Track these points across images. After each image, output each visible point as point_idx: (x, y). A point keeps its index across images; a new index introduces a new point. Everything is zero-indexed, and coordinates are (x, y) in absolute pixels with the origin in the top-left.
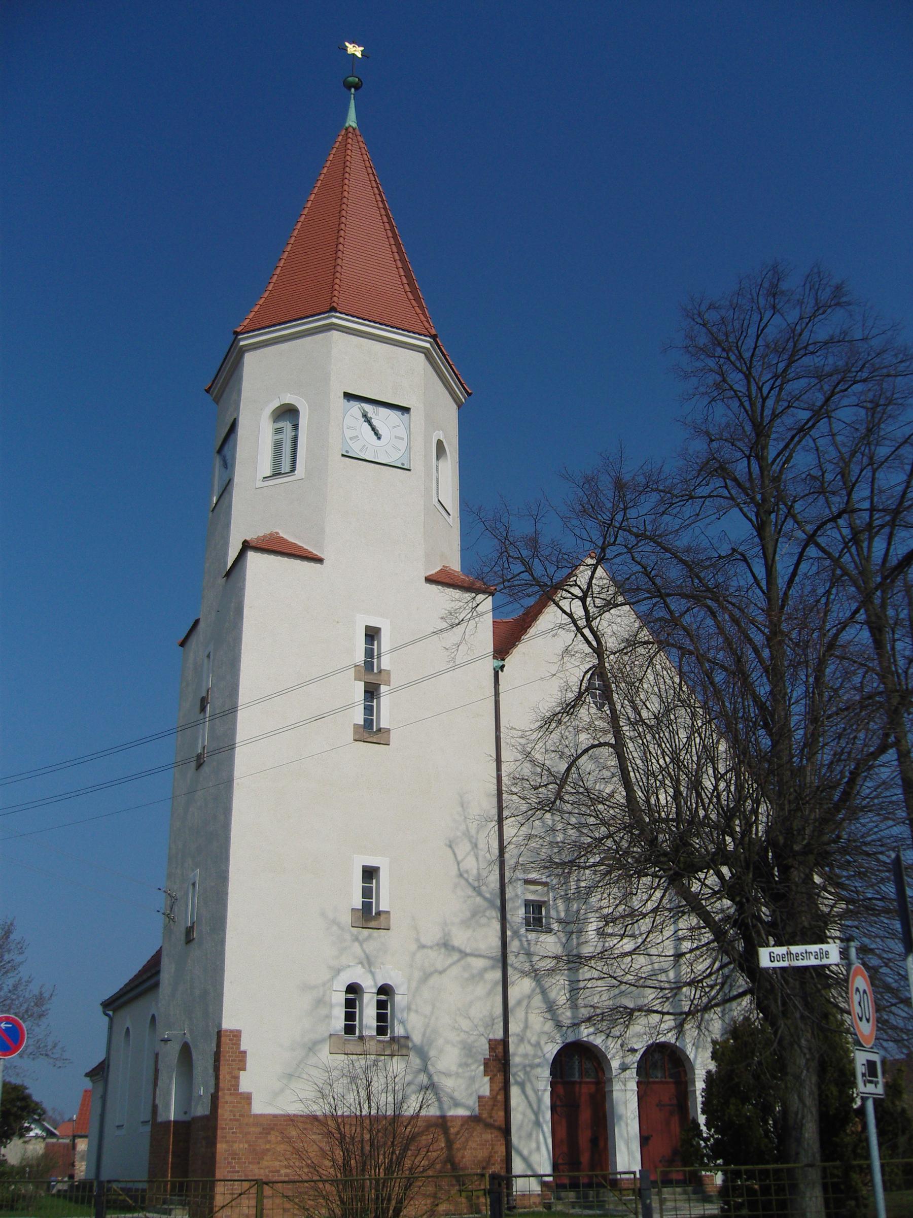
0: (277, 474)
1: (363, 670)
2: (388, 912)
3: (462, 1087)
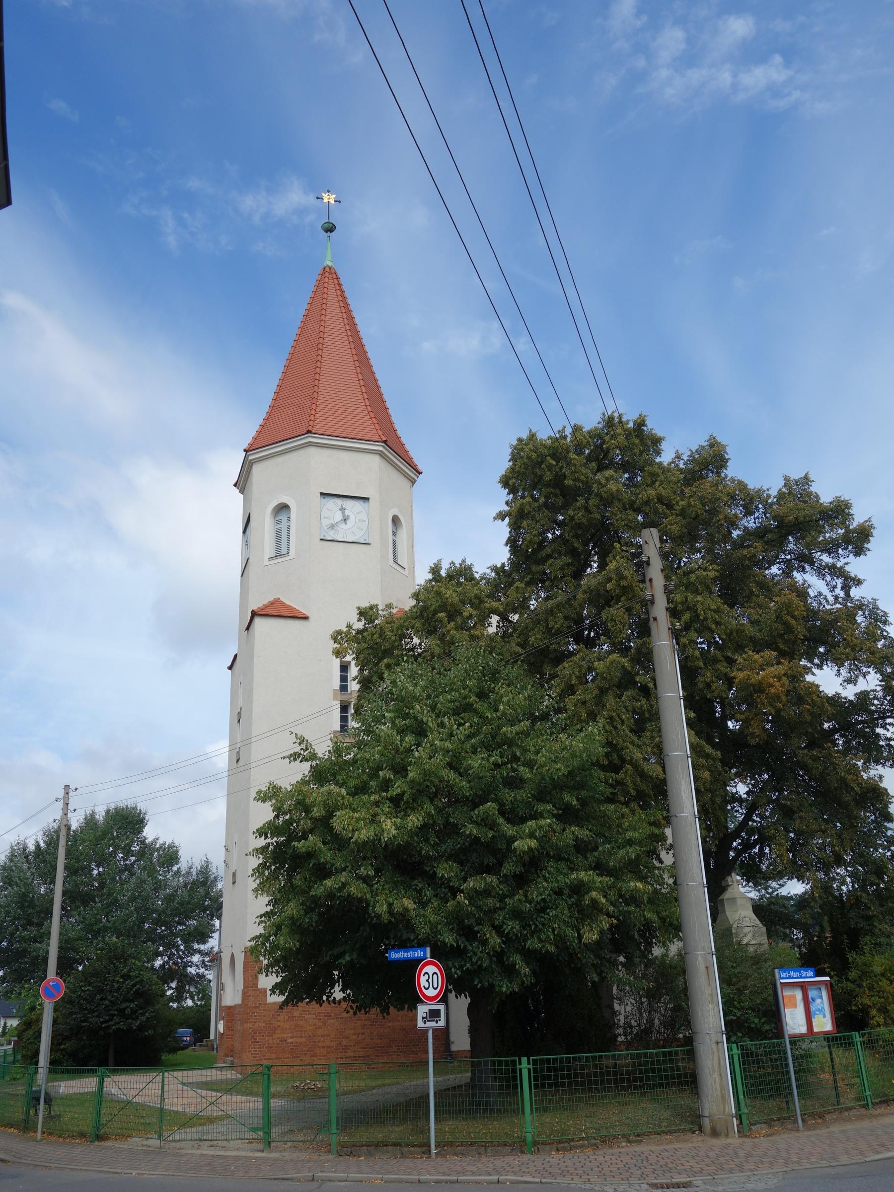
1: (338, 692)
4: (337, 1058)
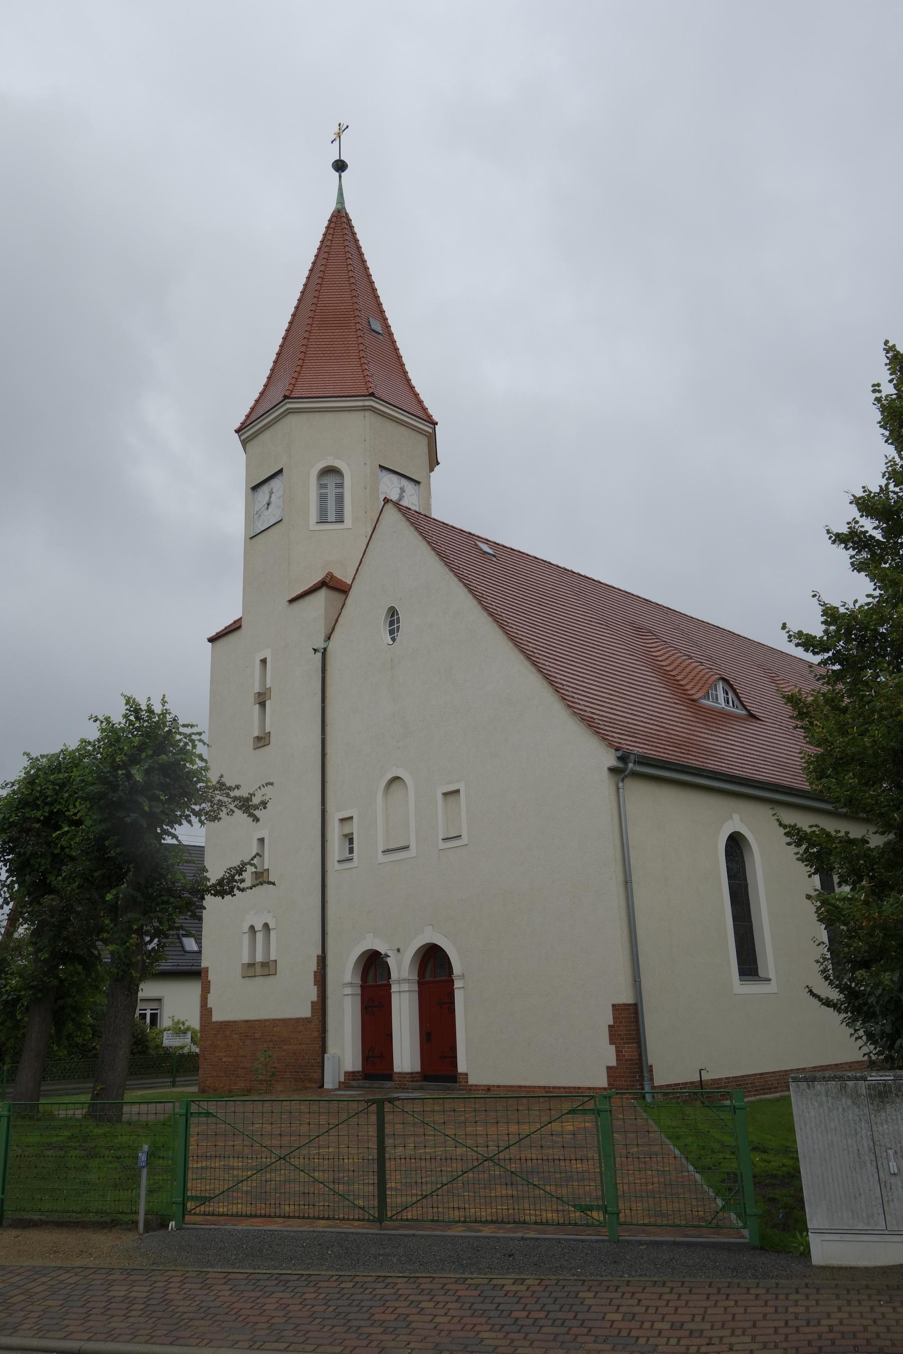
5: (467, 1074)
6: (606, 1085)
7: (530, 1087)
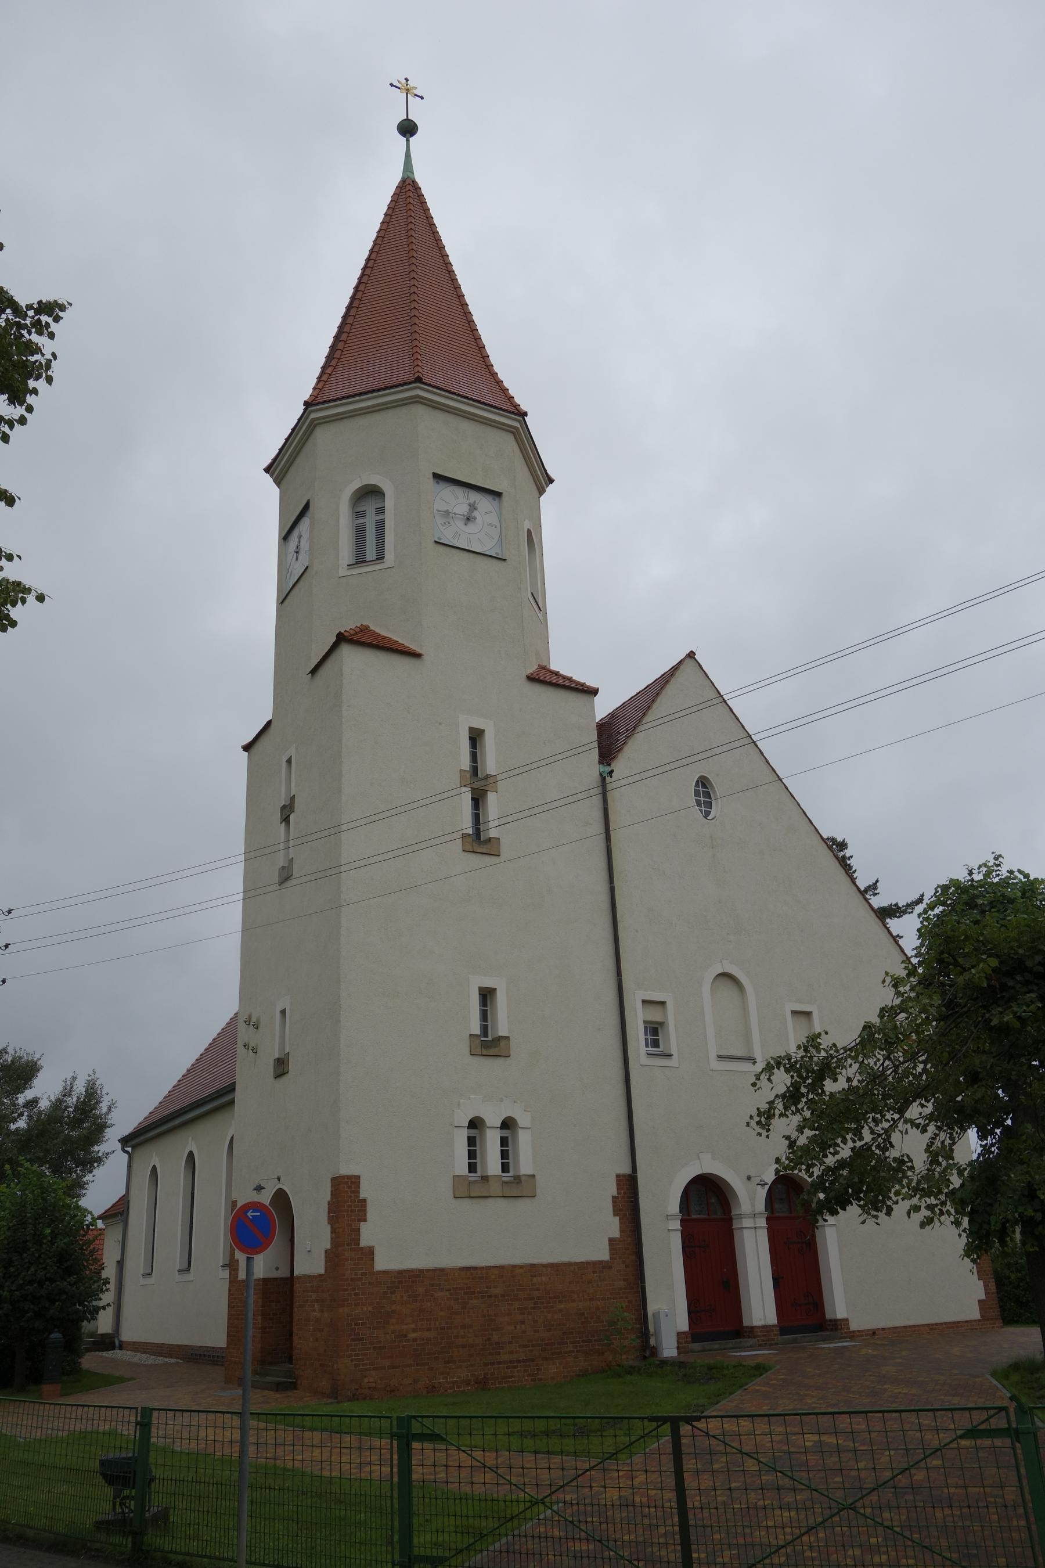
0: (360, 560)
2: (507, 1038)
3: (583, 1235)
4: (486, 1365)
5: (847, 1320)
6: (979, 1317)
7: (914, 1326)
